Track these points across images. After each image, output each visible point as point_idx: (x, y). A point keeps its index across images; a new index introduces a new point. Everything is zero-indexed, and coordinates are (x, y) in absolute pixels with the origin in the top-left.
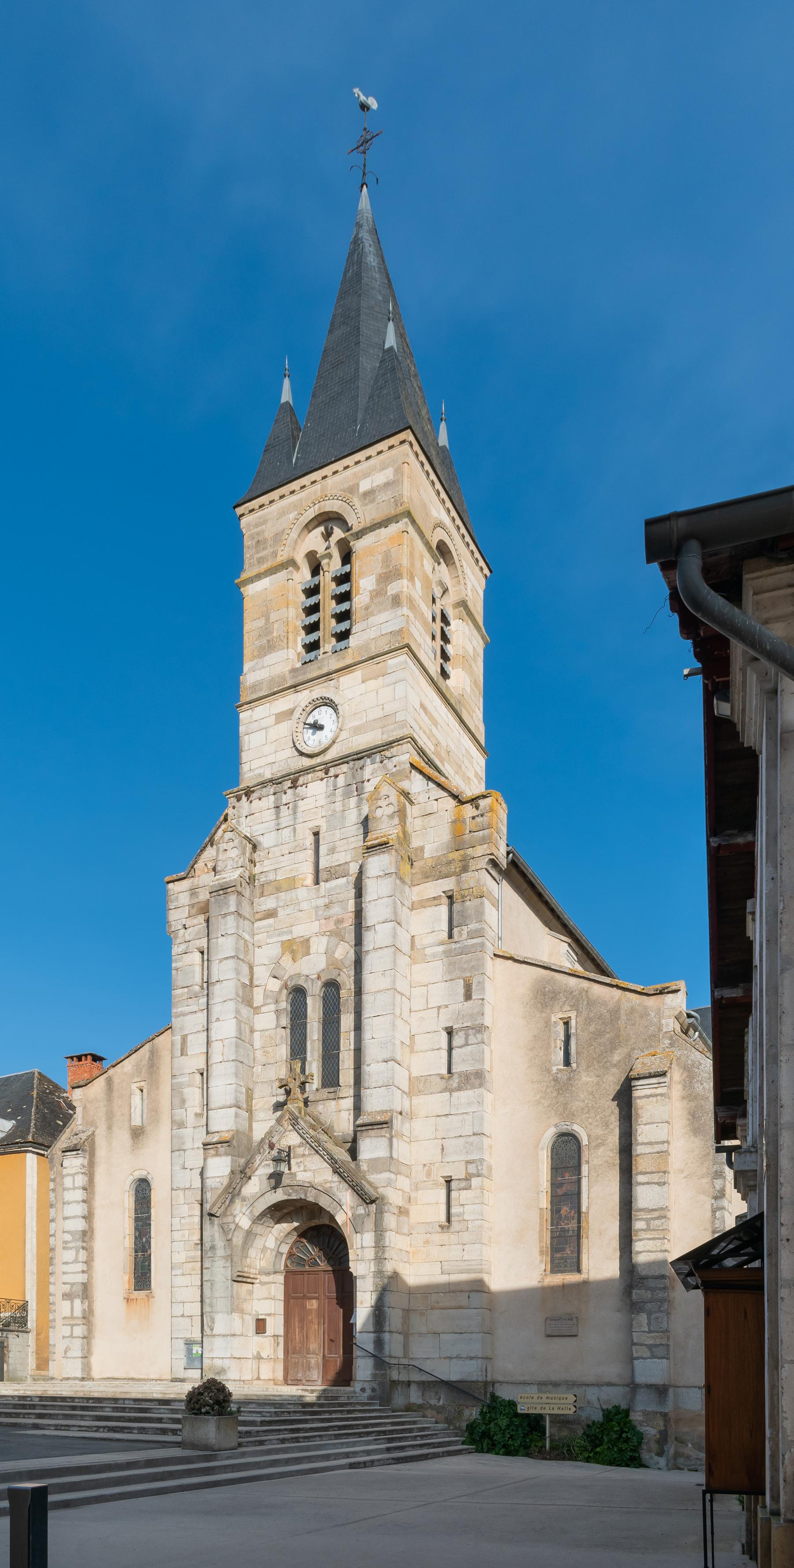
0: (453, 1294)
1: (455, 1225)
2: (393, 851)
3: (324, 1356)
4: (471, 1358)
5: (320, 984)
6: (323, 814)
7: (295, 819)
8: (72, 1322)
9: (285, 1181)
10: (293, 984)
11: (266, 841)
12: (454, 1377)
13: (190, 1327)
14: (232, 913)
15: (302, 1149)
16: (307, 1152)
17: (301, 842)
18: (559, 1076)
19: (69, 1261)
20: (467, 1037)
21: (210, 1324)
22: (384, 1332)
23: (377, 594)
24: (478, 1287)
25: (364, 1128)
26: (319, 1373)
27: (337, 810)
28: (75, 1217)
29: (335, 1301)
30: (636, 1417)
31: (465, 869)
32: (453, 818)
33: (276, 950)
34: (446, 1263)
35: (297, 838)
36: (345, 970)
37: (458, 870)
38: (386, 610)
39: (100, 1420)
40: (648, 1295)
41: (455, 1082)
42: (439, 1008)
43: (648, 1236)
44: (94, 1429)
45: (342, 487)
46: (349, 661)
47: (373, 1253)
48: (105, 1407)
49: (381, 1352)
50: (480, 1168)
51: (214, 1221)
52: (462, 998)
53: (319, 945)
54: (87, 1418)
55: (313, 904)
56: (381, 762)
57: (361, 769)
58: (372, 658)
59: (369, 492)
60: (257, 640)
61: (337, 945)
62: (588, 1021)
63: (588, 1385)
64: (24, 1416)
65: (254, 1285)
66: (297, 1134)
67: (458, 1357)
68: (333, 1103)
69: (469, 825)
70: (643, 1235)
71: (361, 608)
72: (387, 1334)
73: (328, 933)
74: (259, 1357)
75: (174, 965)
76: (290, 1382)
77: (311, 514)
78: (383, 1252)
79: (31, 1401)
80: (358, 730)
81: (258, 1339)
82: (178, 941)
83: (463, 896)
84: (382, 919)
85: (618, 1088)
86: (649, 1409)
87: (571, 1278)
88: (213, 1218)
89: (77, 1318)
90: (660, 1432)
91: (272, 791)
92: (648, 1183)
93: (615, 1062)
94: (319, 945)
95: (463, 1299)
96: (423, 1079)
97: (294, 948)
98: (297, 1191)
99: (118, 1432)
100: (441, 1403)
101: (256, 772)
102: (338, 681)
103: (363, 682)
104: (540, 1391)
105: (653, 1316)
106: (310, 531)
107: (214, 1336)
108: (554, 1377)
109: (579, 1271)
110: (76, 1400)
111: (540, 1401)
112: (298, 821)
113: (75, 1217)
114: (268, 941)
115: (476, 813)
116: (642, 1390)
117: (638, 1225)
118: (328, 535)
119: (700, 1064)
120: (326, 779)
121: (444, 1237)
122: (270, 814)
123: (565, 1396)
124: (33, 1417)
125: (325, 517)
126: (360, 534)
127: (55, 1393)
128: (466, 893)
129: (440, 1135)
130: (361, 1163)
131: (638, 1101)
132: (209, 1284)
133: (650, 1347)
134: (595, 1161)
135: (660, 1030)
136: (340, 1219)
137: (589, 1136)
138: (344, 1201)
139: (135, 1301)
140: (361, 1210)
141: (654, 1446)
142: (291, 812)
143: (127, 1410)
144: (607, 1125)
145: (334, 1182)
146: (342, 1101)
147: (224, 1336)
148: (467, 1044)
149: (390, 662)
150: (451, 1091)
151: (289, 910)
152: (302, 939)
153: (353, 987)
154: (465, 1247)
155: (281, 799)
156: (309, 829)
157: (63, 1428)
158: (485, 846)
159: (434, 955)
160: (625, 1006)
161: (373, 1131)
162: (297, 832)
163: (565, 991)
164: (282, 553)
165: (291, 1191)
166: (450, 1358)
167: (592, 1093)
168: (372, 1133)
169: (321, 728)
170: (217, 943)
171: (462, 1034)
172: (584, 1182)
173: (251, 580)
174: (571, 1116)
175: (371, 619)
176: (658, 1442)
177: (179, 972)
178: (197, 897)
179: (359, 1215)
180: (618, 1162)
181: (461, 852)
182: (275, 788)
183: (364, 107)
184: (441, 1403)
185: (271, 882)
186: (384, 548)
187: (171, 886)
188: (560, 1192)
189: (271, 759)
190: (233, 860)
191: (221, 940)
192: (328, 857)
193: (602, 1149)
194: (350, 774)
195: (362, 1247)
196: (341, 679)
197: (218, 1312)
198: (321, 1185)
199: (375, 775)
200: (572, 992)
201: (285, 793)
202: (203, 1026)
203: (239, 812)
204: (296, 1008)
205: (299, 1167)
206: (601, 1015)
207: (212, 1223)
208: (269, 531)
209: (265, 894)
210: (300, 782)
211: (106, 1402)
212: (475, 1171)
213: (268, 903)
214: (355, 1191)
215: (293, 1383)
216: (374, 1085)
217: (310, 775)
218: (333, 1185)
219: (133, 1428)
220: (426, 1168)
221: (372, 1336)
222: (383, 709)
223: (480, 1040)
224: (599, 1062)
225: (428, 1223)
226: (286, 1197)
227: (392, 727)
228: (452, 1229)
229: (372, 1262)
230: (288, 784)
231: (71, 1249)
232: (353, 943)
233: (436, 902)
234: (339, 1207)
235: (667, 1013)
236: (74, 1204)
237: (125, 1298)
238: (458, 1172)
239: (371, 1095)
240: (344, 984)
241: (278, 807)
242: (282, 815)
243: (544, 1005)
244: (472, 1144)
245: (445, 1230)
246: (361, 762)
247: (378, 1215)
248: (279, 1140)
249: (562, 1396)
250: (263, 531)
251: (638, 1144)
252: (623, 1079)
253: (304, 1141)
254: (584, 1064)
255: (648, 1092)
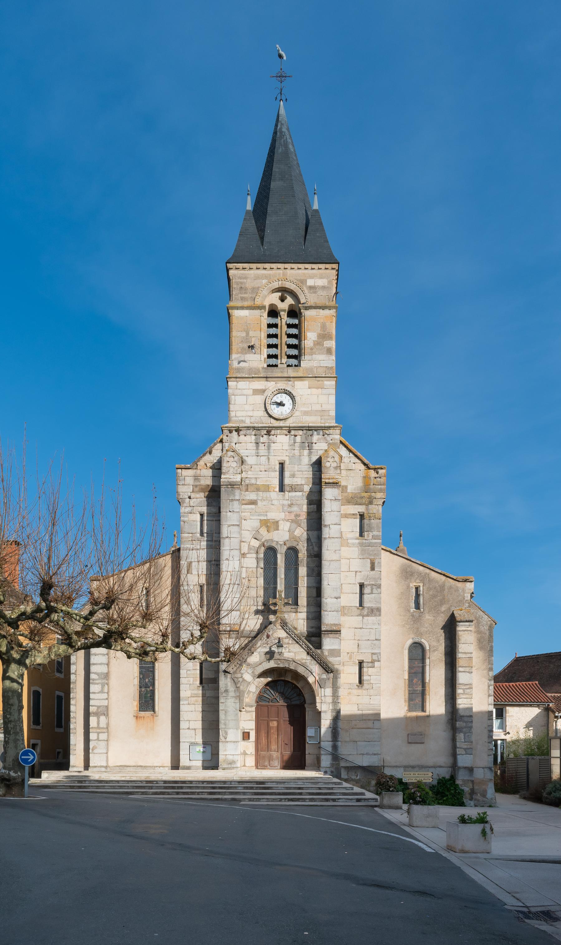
0: (364, 721)
1: (366, 686)
2: (340, 489)
3: (281, 753)
4: (375, 754)
5: (285, 548)
6: (287, 454)
7: (269, 453)
8: (98, 731)
9: (276, 656)
10: (268, 544)
11: (250, 460)
12: (365, 764)
13: (194, 735)
14: (237, 500)
15: (288, 640)
16: (290, 642)
17: (273, 467)
18: (414, 614)
19: (96, 692)
20: (372, 590)
21: (224, 735)
22: (338, 741)
23: (318, 343)
24: (376, 717)
25: (326, 633)
26: (278, 762)
27: (296, 454)
28: (101, 664)
29: (288, 722)
30: (459, 782)
31: (371, 503)
32: (364, 475)
33: (257, 524)
34: (361, 705)
35: (270, 464)
36: (301, 543)
37: (367, 502)
38: (323, 354)
39: (258, 795)
40: (464, 724)
41: (365, 612)
42: (356, 572)
43: (464, 697)
44: (278, 800)
45: (296, 278)
46: (300, 374)
47: (331, 699)
48: (238, 787)
49: (336, 752)
50: (379, 657)
51: (227, 676)
52: (369, 569)
53: (285, 526)
54: (248, 794)
55: (281, 503)
56: (323, 435)
57: (311, 436)
58: (316, 377)
59: (313, 287)
60: (240, 343)
61: (297, 528)
62: (429, 589)
63: (429, 767)
64: (225, 793)
65: (242, 713)
66: (284, 631)
67: (367, 754)
68: (294, 614)
69: (373, 481)
70: (462, 696)
71: (308, 347)
72: (340, 742)
73: (291, 521)
74: (245, 754)
75: (182, 519)
76: (259, 767)
77: (276, 285)
78: (338, 699)
79: (157, 783)
80: (306, 413)
81: (245, 743)
82: (185, 505)
83: (370, 517)
84: (334, 523)
85: (444, 623)
86: (465, 779)
87: (421, 714)
88: (226, 674)
89: (103, 728)
90: (471, 789)
91: (253, 433)
92: (464, 672)
93: (442, 611)
94: (285, 526)
95: (370, 724)
96: (347, 608)
97: (269, 525)
98: (283, 662)
99: (295, 801)
100: (358, 777)
101: (240, 418)
102: (294, 383)
103: (309, 388)
104: (405, 771)
105: (467, 735)
106: (273, 293)
107: (227, 742)
108: (412, 763)
109: (423, 710)
110: (193, 783)
111: (414, 776)
112: (270, 454)
113: (101, 664)
114: (251, 517)
115: (377, 476)
116: (462, 770)
117: (459, 691)
118: (282, 299)
119: (482, 617)
120: (289, 436)
121: (360, 692)
122: (252, 446)
123: (427, 773)
124: (206, 794)
125: (284, 289)
126: (308, 308)
127: (157, 778)
128: (372, 515)
129: (357, 638)
130: (324, 651)
131: (459, 632)
132: (224, 712)
133: (465, 749)
134: (433, 658)
135: (464, 599)
136: (311, 680)
137: (430, 646)
138: (314, 670)
139: (142, 718)
140: (324, 676)
141: (468, 796)
142: (266, 448)
143: (255, 788)
144: (438, 641)
145: (308, 660)
146: (299, 614)
147: (234, 742)
148: (372, 593)
149: (325, 382)
150: (363, 616)
151: (264, 503)
152: (273, 521)
153: (306, 553)
154: (371, 697)
155: (260, 439)
156: (278, 460)
157: (255, 800)
158: (382, 494)
159: (353, 544)
160: (447, 585)
161: (331, 635)
162: (270, 460)
163: (417, 573)
164: (258, 300)
165: (279, 662)
166: (363, 754)
167: (431, 625)
168: (331, 635)
169: (284, 405)
170: (226, 515)
171: (369, 587)
172: (427, 668)
173: (237, 308)
174: (421, 635)
175: (314, 356)
176: (470, 794)
177: (186, 524)
178: (199, 482)
179: (323, 679)
180: (444, 659)
181: (369, 494)
182: (255, 432)
183: (280, 56)
184: (358, 777)
185: (253, 484)
186: (322, 321)
187: (179, 471)
188: (412, 671)
189: (250, 414)
190: (234, 468)
191: (229, 514)
192: (290, 479)
193: (436, 652)
194: (304, 436)
195: (325, 696)
196: (296, 382)
197: (230, 729)
198: (299, 660)
199: (319, 441)
200: (421, 574)
201: (263, 437)
202: (204, 559)
203: (231, 439)
204: (268, 558)
205: (286, 649)
206: (435, 587)
207: (226, 677)
208: (249, 284)
209: (249, 490)
210: (273, 432)
211: (217, 783)
212: (377, 659)
213: (252, 496)
214: (321, 666)
215: (262, 768)
216: (329, 610)
217: (279, 431)
218: (307, 661)
219: (306, 799)
220: (349, 655)
221: (331, 743)
222: (322, 406)
223: (379, 592)
224: (434, 610)
225: (350, 684)
226: (276, 666)
227: (327, 417)
228: (364, 688)
229: (331, 704)
230: (265, 432)
231: (98, 684)
232: (306, 529)
233: (354, 516)
234: (310, 673)
235: (467, 591)
236: (100, 656)
237: (134, 716)
238: (367, 658)
239: (328, 615)
240: (301, 550)
241: (257, 443)
242: (260, 448)
243: (407, 578)
244: (375, 645)
245: (360, 688)
246: (311, 432)
247: (334, 680)
248: (272, 634)
249: (425, 773)
250: (245, 283)
251: (459, 653)
252: (446, 620)
253: (289, 636)
254: (427, 610)
255: (464, 629)
